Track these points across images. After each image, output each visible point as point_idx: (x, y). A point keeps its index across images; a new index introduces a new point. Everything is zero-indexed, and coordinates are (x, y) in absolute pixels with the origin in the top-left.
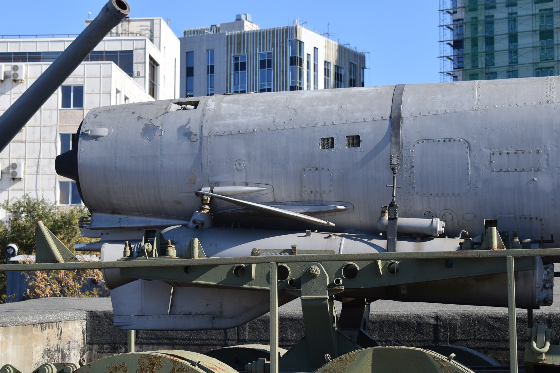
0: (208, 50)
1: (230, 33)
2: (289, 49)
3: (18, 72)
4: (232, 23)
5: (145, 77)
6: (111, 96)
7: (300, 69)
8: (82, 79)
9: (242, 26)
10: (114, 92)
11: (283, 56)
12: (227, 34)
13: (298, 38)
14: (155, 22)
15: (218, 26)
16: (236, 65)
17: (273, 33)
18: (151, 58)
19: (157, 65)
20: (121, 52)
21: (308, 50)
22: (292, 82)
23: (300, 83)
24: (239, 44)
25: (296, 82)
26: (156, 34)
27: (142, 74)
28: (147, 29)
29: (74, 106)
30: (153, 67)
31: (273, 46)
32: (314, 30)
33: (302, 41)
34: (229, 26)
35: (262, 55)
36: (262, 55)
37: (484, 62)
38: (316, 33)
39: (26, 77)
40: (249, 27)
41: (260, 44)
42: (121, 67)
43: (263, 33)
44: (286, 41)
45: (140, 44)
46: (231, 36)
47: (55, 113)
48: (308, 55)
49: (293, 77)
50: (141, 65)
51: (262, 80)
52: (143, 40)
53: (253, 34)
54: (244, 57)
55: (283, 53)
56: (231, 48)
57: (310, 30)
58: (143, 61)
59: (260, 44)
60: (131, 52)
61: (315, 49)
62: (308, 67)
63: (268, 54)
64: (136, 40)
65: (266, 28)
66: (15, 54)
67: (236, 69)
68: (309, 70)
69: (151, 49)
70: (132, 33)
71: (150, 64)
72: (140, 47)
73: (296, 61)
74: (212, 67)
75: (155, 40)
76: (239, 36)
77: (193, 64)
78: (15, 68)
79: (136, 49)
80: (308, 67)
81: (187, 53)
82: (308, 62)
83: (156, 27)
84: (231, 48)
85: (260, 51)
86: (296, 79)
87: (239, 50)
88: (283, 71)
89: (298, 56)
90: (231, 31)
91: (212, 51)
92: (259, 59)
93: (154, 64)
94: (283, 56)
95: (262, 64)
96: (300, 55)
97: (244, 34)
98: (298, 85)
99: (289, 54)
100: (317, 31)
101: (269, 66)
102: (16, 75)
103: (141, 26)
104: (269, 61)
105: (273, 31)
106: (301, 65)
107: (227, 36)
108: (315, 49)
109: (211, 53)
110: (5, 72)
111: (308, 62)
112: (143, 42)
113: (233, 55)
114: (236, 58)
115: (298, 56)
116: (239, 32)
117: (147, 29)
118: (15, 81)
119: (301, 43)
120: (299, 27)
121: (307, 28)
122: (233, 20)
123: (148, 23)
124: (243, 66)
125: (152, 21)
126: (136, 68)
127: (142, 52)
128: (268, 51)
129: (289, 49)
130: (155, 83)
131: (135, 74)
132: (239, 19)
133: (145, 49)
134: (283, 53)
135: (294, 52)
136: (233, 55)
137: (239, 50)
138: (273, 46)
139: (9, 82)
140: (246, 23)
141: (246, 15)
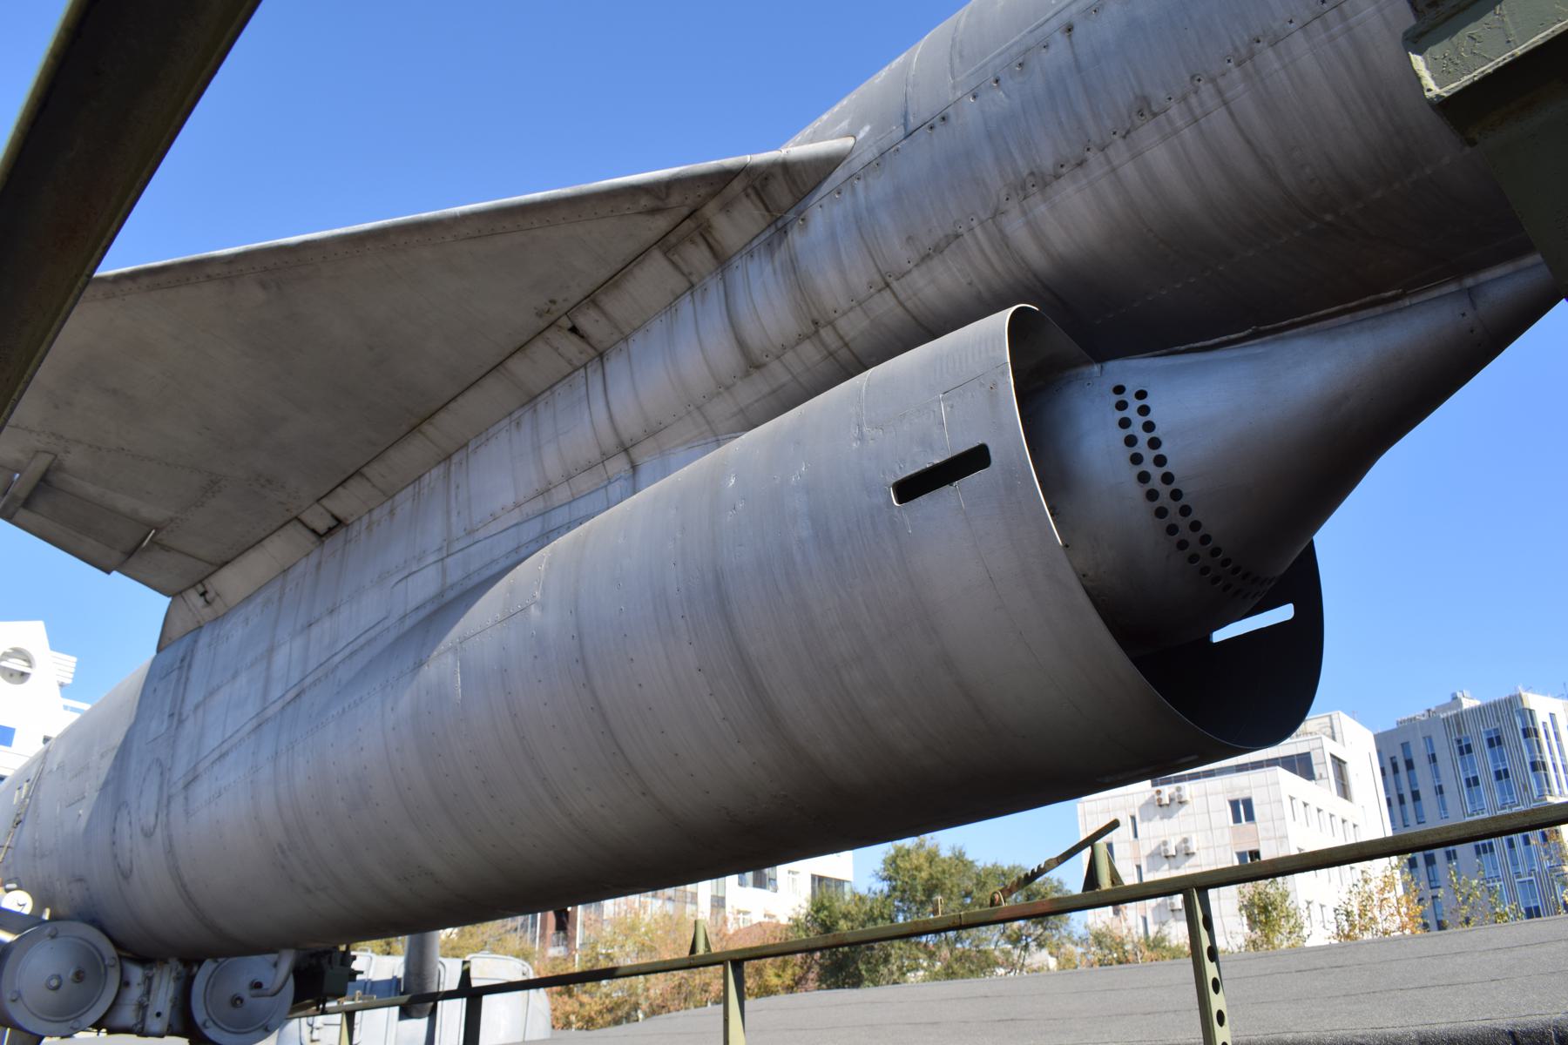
0: (1424, 738)
1: (1445, 715)
2: (1518, 720)
3: (1161, 796)
4: (1449, 704)
5: (1328, 778)
6: (1282, 805)
7: (1538, 741)
8: (1248, 791)
9: (1460, 704)
10: (1287, 801)
11: (1512, 729)
12: (1442, 716)
13: (1526, 706)
14: (1333, 717)
15: (1433, 709)
16: (1461, 749)
17: (1495, 706)
18: (1332, 756)
19: (1344, 763)
20: (1298, 755)
21: (1541, 717)
22: (1531, 758)
23: (1541, 757)
24: (1458, 725)
25: (1536, 757)
26: (1337, 729)
27: (1324, 775)
28: (1325, 727)
29: (1247, 820)
30: (1340, 766)
31: (1498, 720)
32: (1545, 694)
33: (1531, 708)
34: (1444, 708)
35: (1488, 733)
36: (1488, 733)
37: (556, 954)
38: (1354, 719)
39: (1191, 797)
40: (1468, 703)
41: (1482, 721)
42: (1301, 775)
43: (1483, 707)
44: (1512, 712)
45: (1317, 744)
46: (1447, 718)
47: (1226, 830)
48: (1544, 724)
49: (1531, 751)
50: (1321, 766)
51: (1495, 760)
52: (1317, 738)
53: (1473, 711)
54: (1467, 739)
55: (1511, 725)
56: (1450, 730)
57: (1538, 694)
58: (1323, 761)
59: (1482, 721)
60: (1309, 753)
61: (1552, 715)
62: (1547, 737)
63: (1494, 730)
64: (1300, 742)
65: (1488, 701)
66: (1252, 763)
67: (1462, 753)
68: (1341, 781)
69: (1331, 747)
70: (1311, 733)
71: (1333, 762)
72: (1317, 746)
73: (1529, 732)
74: (1434, 755)
75: (1338, 736)
76: (1456, 716)
77: (1410, 754)
78: (1179, 789)
79: (1313, 749)
80: (1547, 737)
81: (1402, 745)
82: (1546, 732)
83: (1335, 722)
84: (1450, 730)
85: (1484, 728)
86: (1535, 752)
87: (1460, 732)
88: (1517, 747)
89: (1531, 726)
90: (1446, 712)
91: (1430, 738)
92: (1485, 737)
93: (1339, 764)
94: (1512, 729)
95: (1491, 743)
96: (1533, 724)
97: (1462, 714)
98: (1539, 759)
99: (1520, 726)
100: (1356, 715)
101: (1499, 743)
102: (1180, 796)
103: (1320, 724)
104: (1498, 738)
105: (1495, 705)
106: (1537, 736)
107: (1443, 719)
108: (1552, 715)
109: (1429, 740)
110: (1169, 796)
111: (1546, 732)
112: (1319, 741)
113: (1453, 738)
114: (1459, 741)
115: (1531, 726)
116: (1455, 712)
117: (1325, 727)
118: (1181, 803)
119: (1531, 711)
120: (1523, 694)
121: (1534, 693)
122: (1448, 699)
123: (1327, 720)
124: (1469, 749)
125: (1330, 716)
126: (1317, 770)
127: (1320, 751)
128: (1494, 727)
129: (1518, 720)
130: (1346, 783)
131: (1317, 776)
132: (1455, 698)
133: (1322, 748)
134: (1511, 725)
135: (1524, 722)
136: (1453, 738)
137: (1460, 732)
138: (1498, 720)
139: (1174, 805)
140: (1463, 700)
141: (1462, 692)
